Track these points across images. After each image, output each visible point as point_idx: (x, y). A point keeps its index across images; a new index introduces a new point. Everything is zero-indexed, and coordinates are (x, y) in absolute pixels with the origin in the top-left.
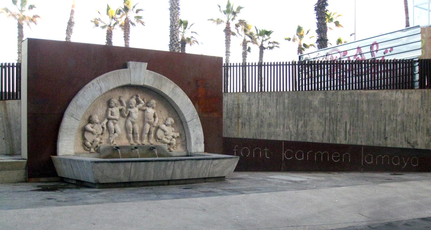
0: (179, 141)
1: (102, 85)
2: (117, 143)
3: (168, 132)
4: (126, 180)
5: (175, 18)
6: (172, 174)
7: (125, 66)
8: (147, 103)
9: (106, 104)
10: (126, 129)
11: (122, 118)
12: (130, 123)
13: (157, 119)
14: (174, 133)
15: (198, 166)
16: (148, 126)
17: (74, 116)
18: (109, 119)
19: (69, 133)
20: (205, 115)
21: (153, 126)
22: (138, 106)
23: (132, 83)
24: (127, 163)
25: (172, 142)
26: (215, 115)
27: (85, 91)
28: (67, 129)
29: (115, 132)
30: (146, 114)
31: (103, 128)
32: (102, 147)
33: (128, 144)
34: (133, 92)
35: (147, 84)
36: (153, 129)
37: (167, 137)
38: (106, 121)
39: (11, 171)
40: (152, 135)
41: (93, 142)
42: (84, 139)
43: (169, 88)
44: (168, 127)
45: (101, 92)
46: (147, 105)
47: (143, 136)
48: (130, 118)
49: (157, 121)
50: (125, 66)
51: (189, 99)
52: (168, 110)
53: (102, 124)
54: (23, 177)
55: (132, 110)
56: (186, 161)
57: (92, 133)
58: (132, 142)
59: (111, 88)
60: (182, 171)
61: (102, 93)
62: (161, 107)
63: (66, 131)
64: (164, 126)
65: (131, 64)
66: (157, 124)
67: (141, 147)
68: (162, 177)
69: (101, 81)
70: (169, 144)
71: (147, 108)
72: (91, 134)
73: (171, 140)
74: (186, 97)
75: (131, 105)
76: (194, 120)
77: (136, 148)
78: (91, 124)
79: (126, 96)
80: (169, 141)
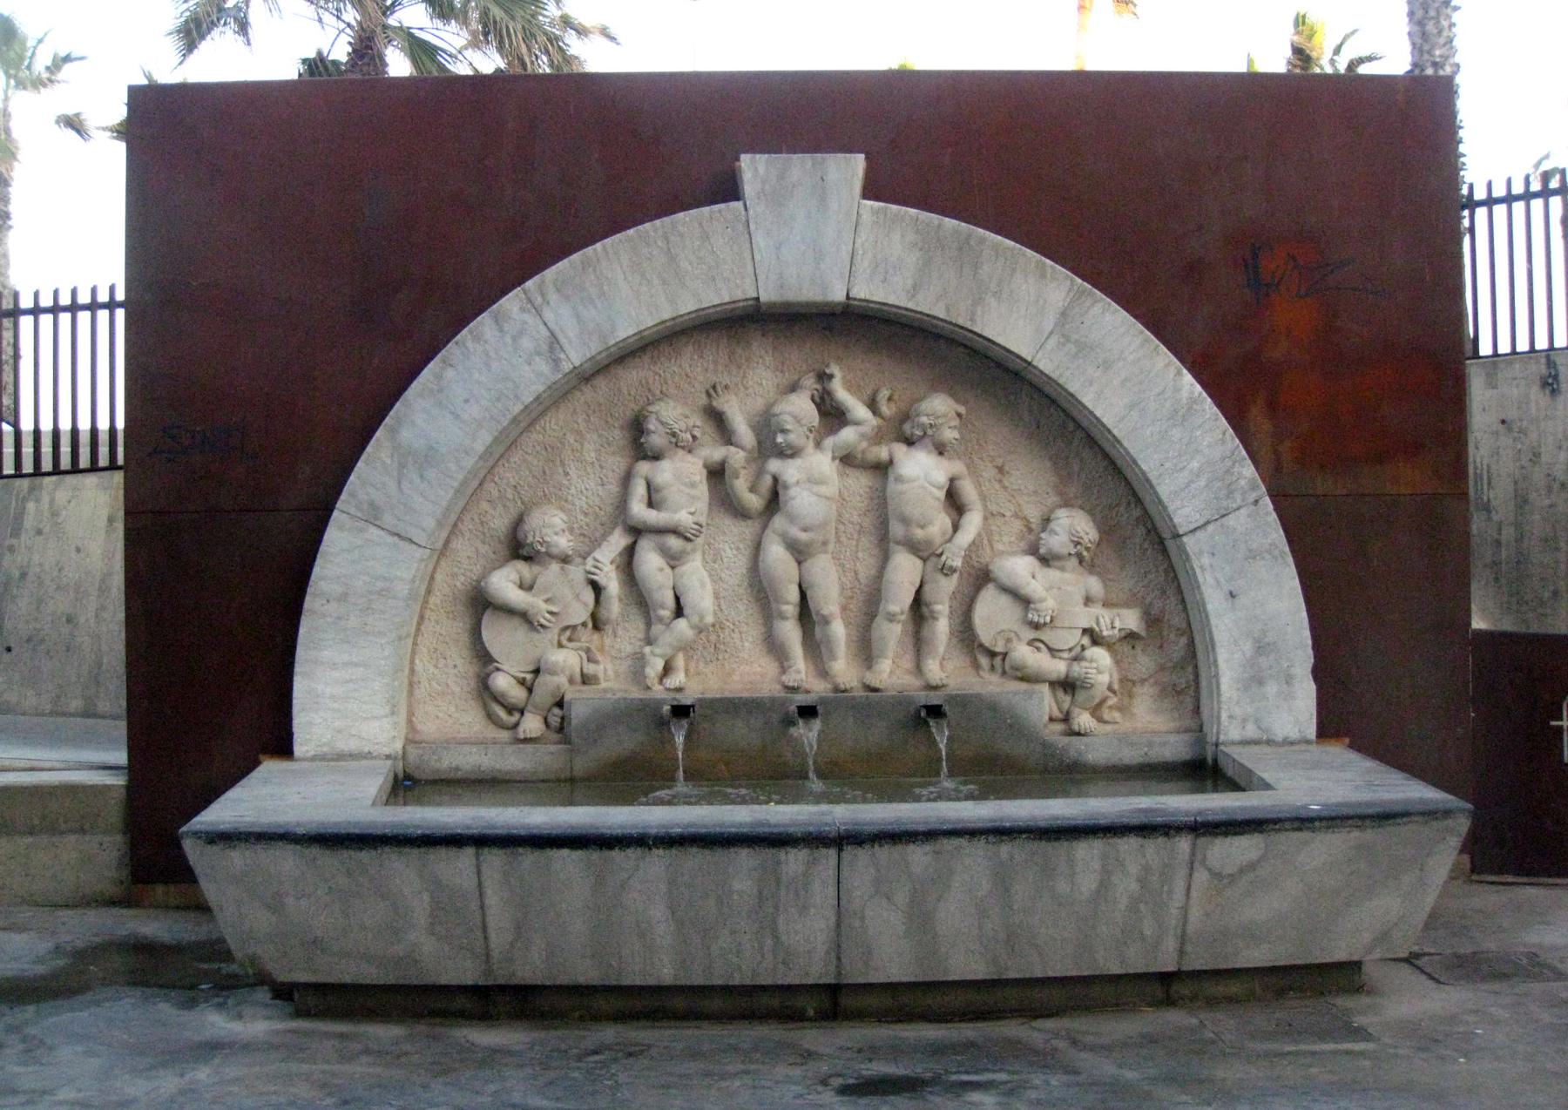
0: (1144, 663)
1: (560, 315)
2: (691, 683)
4: (462, 971)
5: (1430, 27)
6: (837, 949)
7: (728, 189)
8: (905, 417)
9: (618, 436)
10: (761, 590)
12: (776, 554)
13: (973, 523)
14: (1097, 610)
15: (1062, 886)
16: (905, 571)
17: (388, 519)
18: (637, 531)
19: (353, 621)
20: (1323, 484)
21: (946, 571)
22: (829, 442)
23: (768, 295)
24: (442, 852)
25: (1078, 670)
26: (1407, 480)
27: (447, 363)
28: (343, 598)
29: (679, 612)
30: (892, 487)
31: (597, 588)
32: (582, 704)
34: (800, 355)
35: (869, 290)
36: (943, 592)
37: (1046, 635)
38: (618, 541)
39: (44, 839)
40: (942, 628)
41: (537, 672)
42: (484, 658)
43: (1033, 307)
44: (1053, 574)
47: (875, 634)
48: (778, 522)
49: (966, 536)
50: (728, 189)
51: (1188, 378)
52: (1060, 465)
53: (590, 561)
54: (112, 873)
55: (790, 471)
56: (948, 844)
57: (524, 617)
58: (800, 669)
59: (625, 331)
60: (920, 919)
61: (566, 367)
62: (998, 435)
63: (333, 607)
64: (1019, 568)
65: (753, 169)
66: (975, 545)
68: (740, 959)
69: (553, 297)
70: (1068, 685)
71: (900, 450)
72: (516, 621)
74: (1164, 361)
75: (780, 439)
76: (1231, 521)
77: (808, 712)
78: (520, 565)
79: (758, 385)
80: (1058, 668)
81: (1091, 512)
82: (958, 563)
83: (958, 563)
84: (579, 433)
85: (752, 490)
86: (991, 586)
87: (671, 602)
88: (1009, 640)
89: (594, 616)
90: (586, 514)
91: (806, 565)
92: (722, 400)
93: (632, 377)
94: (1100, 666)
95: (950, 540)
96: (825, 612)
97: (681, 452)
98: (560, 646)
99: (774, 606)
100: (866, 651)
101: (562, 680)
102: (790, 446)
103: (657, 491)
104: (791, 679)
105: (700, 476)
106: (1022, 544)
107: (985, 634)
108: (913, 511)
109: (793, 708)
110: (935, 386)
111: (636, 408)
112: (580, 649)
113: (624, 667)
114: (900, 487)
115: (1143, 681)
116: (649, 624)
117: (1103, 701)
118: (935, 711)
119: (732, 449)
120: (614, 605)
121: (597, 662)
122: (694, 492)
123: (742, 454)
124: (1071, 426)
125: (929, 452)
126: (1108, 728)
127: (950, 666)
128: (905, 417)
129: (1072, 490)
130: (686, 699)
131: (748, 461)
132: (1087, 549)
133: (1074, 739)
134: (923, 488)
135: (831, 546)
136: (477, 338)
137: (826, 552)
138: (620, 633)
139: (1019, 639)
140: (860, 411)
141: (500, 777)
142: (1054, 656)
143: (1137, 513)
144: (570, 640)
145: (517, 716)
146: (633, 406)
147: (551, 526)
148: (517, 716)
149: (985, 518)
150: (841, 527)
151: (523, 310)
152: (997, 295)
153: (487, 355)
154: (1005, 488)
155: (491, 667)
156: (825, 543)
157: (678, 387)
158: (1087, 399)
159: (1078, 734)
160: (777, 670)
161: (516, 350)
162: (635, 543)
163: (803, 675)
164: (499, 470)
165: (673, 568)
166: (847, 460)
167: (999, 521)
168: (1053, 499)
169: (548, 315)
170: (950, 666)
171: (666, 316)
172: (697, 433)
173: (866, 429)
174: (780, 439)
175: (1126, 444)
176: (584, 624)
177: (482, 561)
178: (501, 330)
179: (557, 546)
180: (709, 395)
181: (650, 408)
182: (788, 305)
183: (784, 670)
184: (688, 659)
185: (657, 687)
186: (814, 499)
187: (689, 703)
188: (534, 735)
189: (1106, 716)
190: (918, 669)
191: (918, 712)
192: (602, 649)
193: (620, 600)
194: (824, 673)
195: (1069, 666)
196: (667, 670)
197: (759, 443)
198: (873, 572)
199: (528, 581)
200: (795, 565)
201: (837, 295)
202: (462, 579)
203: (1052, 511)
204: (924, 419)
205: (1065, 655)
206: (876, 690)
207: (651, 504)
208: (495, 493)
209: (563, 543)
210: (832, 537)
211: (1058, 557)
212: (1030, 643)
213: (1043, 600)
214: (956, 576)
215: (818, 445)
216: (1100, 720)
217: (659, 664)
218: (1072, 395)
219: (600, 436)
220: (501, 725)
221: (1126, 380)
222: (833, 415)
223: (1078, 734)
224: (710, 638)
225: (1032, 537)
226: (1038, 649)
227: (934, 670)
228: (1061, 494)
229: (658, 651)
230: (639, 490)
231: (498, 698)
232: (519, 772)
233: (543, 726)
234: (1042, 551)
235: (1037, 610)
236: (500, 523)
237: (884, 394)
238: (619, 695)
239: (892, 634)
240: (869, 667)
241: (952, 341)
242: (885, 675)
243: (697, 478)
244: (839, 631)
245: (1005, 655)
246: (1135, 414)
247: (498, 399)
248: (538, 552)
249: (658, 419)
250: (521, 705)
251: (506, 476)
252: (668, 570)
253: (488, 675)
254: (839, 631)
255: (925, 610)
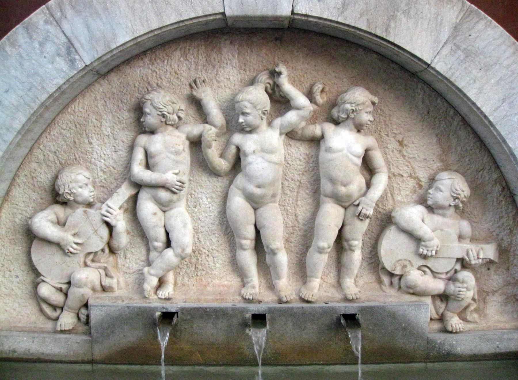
0: (496, 280)
2: (176, 295)
3: (436, 242)
8: (333, 104)
9: (127, 116)
10: (228, 229)
11: (205, 179)
12: (238, 203)
13: (381, 181)
14: (467, 245)
16: (331, 216)
18: (139, 186)
21: (361, 217)
22: (278, 122)
25: (452, 288)
29: (168, 244)
30: (323, 155)
33: (232, 301)
34: (257, 58)
36: (359, 233)
38: (125, 192)
40: (357, 257)
41: (69, 283)
44: (437, 219)
45: (72, 62)
46: (332, 114)
48: (240, 180)
52: (443, 139)
53: (104, 207)
55: (249, 143)
61: (80, 65)
62: (400, 118)
64: (413, 215)
66: (383, 198)
67: (290, 313)
69: (69, 13)
70: (444, 297)
71: (329, 128)
72: (54, 249)
73: (452, 279)
75: (241, 120)
77: (259, 319)
78: (58, 209)
79: (229, 80)
80: (438, 286)
81: (463, 174)
82: (370, 212)
83: (370, 212)
84: (98, 113)
85: (222, 156)
86: (393, 227)
87: (162, 237)
88: (405, 266)
89: (109, 244)
90: (104, 172)
91: (259, 211)
92: (200, 90)
93: (139, 72)
94: (468, 285)
95: (364, 194)
96: (273, 246)
97: (170, 128)
98: (86, 265)
99: (237, 240)
100: (302, 270)
101: (86, 291)
102: (249, 125)
103: (152, 157)
104: (248, 293)
105: (183, 146)
106: (414, 196)
107: (388, 260)
108: (339, 174)
109: (248, 315)
110: (355, 83)
111: (139, 96)
112: (100, 267)
113: (131, 279)
114: (330, 156)
115: (494, 292)
116: (148, 250)
117: (467, 307)
118: (352, 319)
119: (207, 126)
120: (123, 239)
121: (111, 277)
122: (178, 158)
123: (214, 130)
124: (452, 112)
125: (351, 130)
126: (471, 326)
127: (361, 282)
128: (333, 104)
129: (452, 158)
130: (172, 308)
131: (218, 135)
132: (462, 202)
133: (449, 335)
134: (347, 157)
135: (278, 198)
136: (13, 44)
137: (275, 202)
138: (129, 256)
139: (412, 266)
140: (300, 99)
141: (42, 357)
142: (435, 277)
143: (495, 176)
144: (93, 261)
145: (59, 311)
146: (137, 94)
147: (77, 182)
148: (59, 311)
149: (389, 178)
150: (286, 183)
151: (46, 22)
152: (406, 13)
153: (21, 57)
154: (404, 156)
155: (39, 280)
156: (274, 196)
157: (170, 82)
158: (471, 94)
159: (451, 332)
160: (240, 284)
161: (42, 52)
162: (138, 193)
163: (257, 290)
164: (43, 140)
165: (164, 212)
166: (291, 135)
167: (399, 180)
168: (437, 165)
169: (66, 26)
170: (361, 282)
171: (155, 26)
172: (182, 115)
173: (306, 113)
174: (241, 120)
175: (498, 127)
176: (103, 250)
177: (33, 205)
178: (31, 38)
179: (81, 195)
180: (191, 87)
181: (147, 97)
182: (246, 19)
183: (244, 285)
184: (177, 274)
185: (154, 297)
186: (266, 165)
187: (173, 310)
188: (67, 328)
189: (469, 318)
190: (339, 284)
191: (339, 320)
192: (116, 266)
193: (128, 233)
194: (272, 287)
195: (447, 285)
196: (161, 283)
197: (227, 122)
198: (308, 215)
199: (62, 220)
200: (252, 211)
201: (285, 11)
202: (20, 216)
203: (436, 174)
204: (348, 106)
205: (443, 276)
206: (308, 302)
207: (148, 166)
208: (41, 157)
209: (87, 193)
210: (280, 191)
211: (441, 207)
212: (419, 269)
213: (430, 240)
214: (368, 221)
215: (270, 124)
216: (464, 320)
217: (155, 281)
218: (460, 90)
219: (114, 116)
220: (49, 318)
221: (501, 79)
222: (281, 102)
223: (451, 332)
224: (191, 262)
225: (421, 192)
226: (424, 272)
227: (351, 287)
228: (442, 161)
229: (152, 272)
230: (139, 156)
231: (45, 301)
232: (55, 355)
233: (75, 320)
234: (430, 202)
235: (426, 246)
236: (44, 177)
237: (318, 87)
238: (126, 303)
239: (321, 261)
240: (305, 283)
241: (368, 50)
242: (316, 291)
243: (181, 148)
244: (283, 259)
245: (401, 277)
246: (506, 106)
247: (30, 90)
248: (69, 200)
249: (152, 104)
250: (61, 305)
251: (49, 144)
252: (160, 213)
253: (38, 284)
254: (283, 259)
255: (345, 244)
